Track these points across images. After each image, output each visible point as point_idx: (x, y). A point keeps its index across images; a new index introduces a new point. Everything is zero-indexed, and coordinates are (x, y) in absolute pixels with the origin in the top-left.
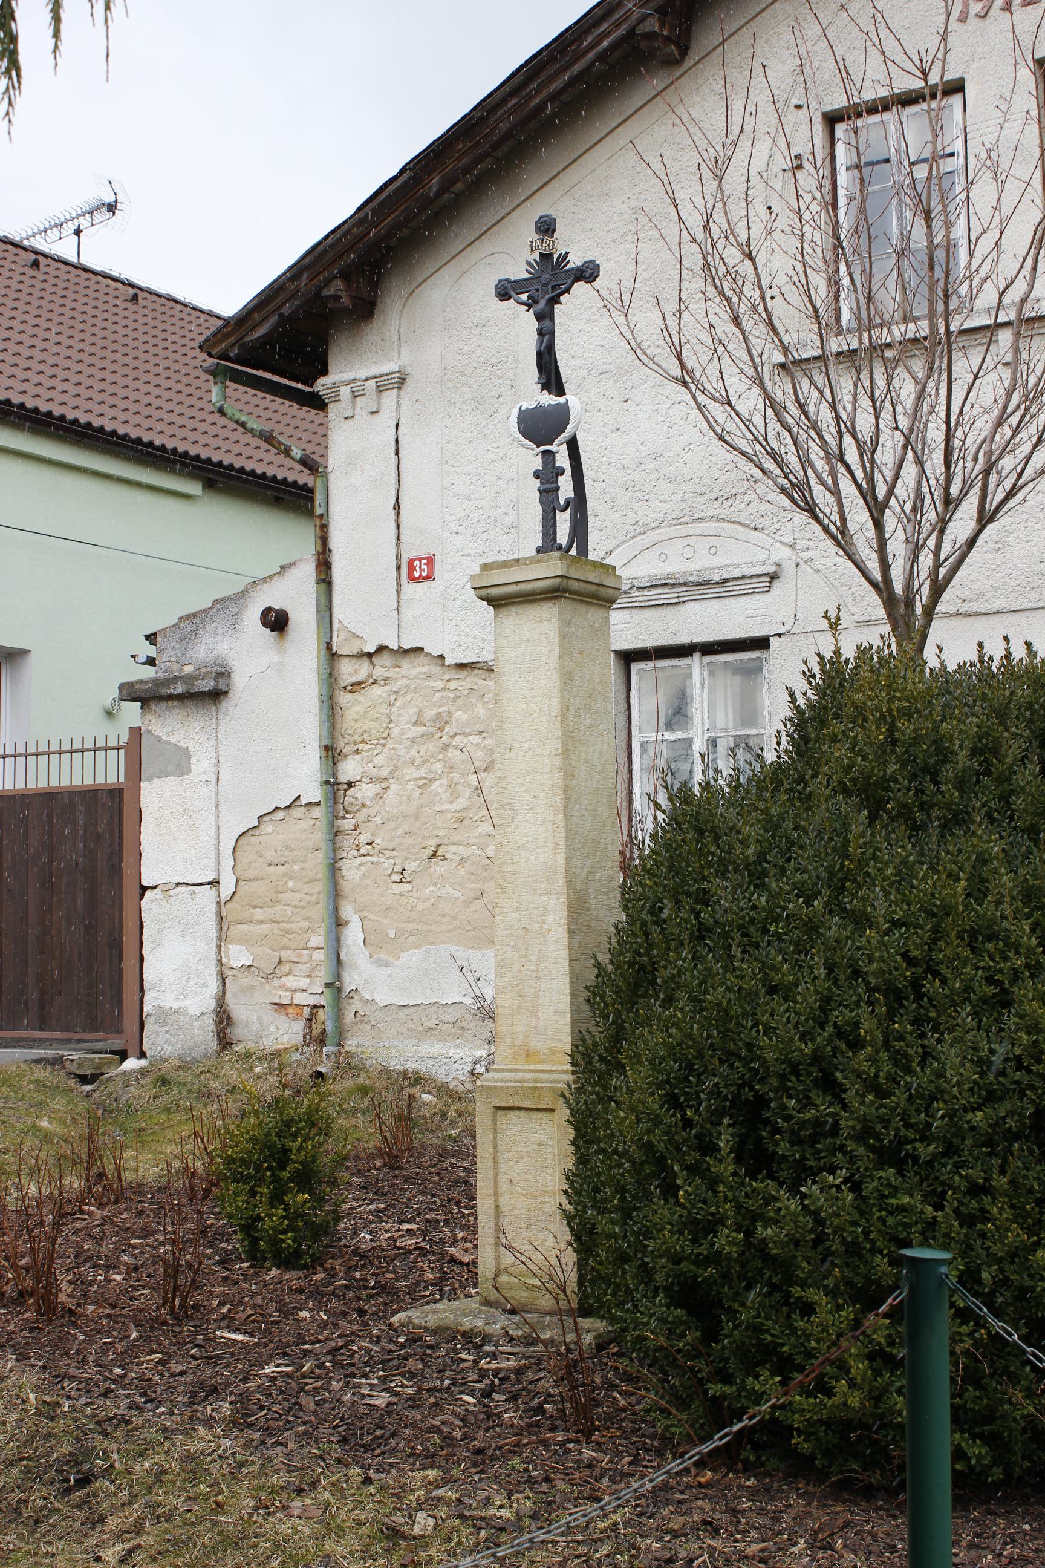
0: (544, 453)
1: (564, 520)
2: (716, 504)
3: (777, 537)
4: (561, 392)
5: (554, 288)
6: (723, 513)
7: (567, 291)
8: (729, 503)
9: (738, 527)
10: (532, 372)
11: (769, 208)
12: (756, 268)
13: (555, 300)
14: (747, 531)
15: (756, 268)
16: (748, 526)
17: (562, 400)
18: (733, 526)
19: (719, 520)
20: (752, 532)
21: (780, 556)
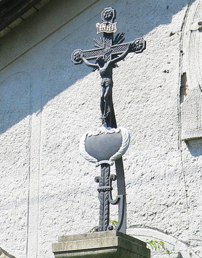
0: (103, 165)
1: (114, 210)
2: (144, 218)
3: (179, 238)
4: (114, 125)
5: (113, 56)
6: (148, 223)
7: (122, 58)
8: (152, 217)
9: (156, 231)
10: (98, 113)
11: (182, 52)
12: (28, 210)
13: (113, 65)
14: (161, 233)
15: (28, 210)
16: (162, 231)
17: (117, 130)
18: (154, 231)
19: (145, 227)
20: (164, 234)
21: (180, 249)
